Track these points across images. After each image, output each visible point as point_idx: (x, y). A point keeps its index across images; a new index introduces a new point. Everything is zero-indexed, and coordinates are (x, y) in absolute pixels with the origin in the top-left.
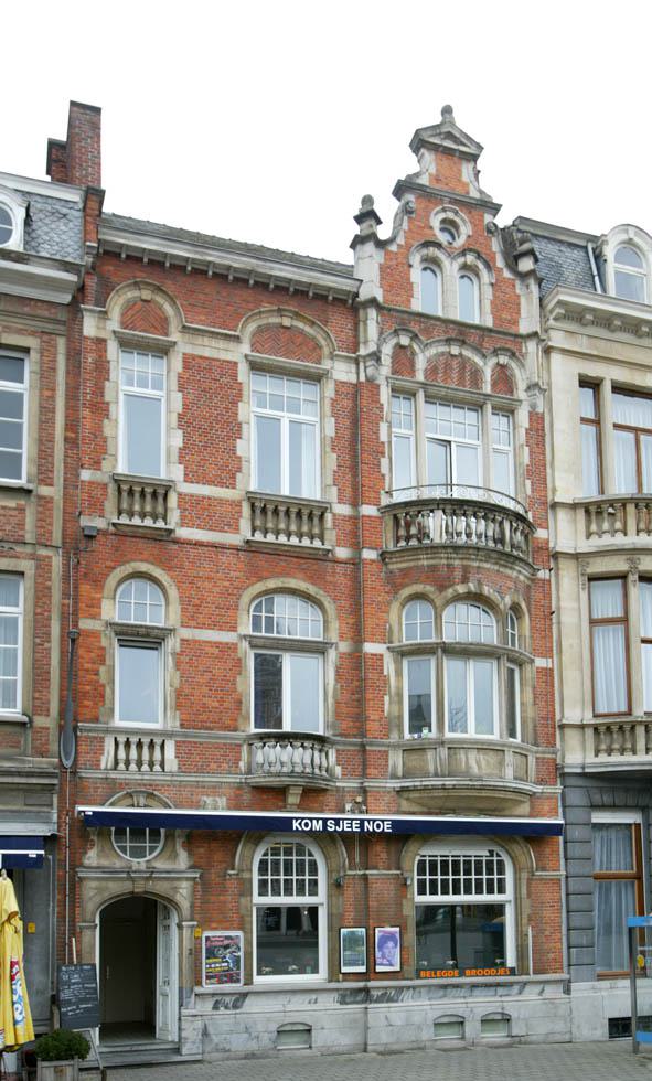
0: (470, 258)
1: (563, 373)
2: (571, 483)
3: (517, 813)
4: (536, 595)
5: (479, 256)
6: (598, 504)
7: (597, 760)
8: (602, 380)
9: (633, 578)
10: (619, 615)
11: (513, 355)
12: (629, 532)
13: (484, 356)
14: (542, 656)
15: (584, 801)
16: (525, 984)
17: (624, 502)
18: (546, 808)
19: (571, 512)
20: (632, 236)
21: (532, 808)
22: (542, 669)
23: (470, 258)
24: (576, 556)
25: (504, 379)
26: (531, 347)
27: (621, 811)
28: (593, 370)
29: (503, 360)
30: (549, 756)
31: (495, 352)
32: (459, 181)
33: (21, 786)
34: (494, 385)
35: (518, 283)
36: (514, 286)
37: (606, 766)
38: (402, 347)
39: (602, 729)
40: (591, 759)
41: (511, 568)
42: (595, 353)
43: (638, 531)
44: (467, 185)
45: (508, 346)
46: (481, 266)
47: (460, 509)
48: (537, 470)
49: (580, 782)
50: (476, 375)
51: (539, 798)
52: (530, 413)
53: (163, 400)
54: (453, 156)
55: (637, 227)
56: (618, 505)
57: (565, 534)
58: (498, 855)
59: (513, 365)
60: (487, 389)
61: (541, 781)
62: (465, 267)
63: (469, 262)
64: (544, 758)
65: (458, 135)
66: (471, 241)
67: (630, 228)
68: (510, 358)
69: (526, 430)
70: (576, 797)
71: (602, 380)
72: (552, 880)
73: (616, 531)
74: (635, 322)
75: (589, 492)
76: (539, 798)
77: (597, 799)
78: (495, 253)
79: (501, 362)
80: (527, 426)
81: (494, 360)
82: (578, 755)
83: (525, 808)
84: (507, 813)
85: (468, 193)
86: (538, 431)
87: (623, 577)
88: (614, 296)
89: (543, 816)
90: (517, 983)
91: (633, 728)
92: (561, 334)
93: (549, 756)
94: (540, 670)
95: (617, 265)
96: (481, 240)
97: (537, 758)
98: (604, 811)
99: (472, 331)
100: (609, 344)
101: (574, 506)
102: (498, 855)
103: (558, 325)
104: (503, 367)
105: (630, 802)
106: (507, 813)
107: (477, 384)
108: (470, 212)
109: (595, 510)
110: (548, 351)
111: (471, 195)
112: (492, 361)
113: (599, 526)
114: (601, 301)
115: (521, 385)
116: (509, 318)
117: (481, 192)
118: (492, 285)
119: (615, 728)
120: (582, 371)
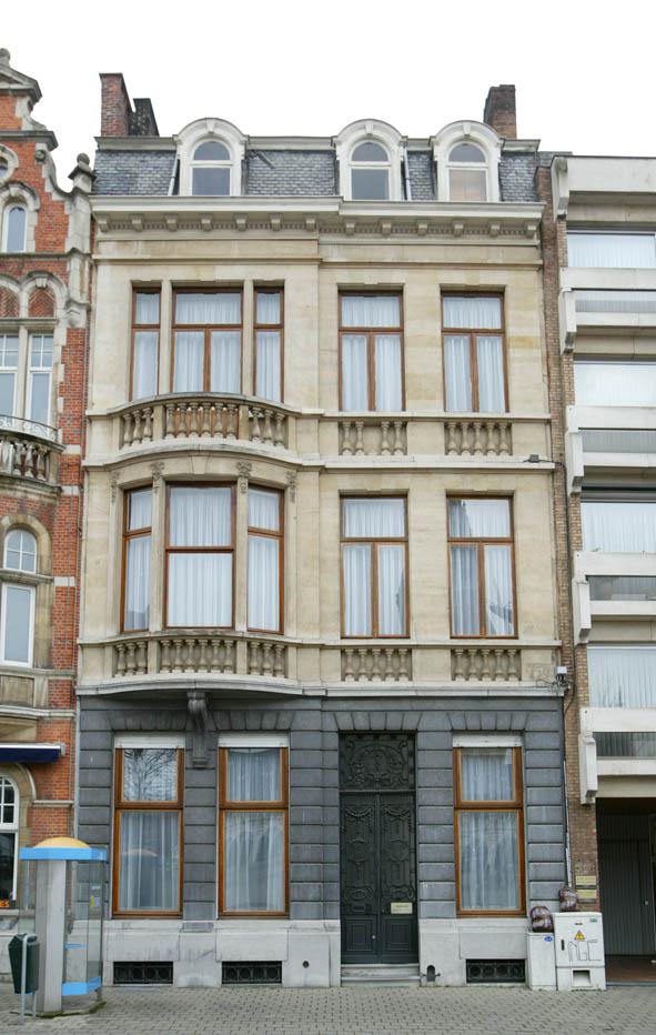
0: (14, 190)
1: (112, 287)
2: (105, 396)
3: (21, 738)
4: (62, 513)
5: (23, 186)
6: (129, 410)
7: (343, 684)
8: (160, 282)
9: (242, 482)
10: (505, 536)
11: (51, 276)
12: (155, 437)
13: (18, 283)
14: (63, 574)
15: (104, 725)
16: (17, 918)
17: (151, 405)
18: (57, 733)
19: (107, 423)
20: (211, 129)
21: (39, 733)
22: (63, 588)
23: (14, 190)
24: (107, 468)
25: (43, 301)
26: (75, 264)
27: (161, 735)
28: (146, 275)
29: (41, 282)
30: (65, 678)
31: (30, 276)
32: (11, 118)
33: (253, 751)
34: (32, 309)
35: (67, 205)
36: (63, 207)
37: (116, 687)
38: (42, 289)
39: (255, 645)
40: (108, 680)
41: (11, 489)
42: (148, 257)
43: (165, 434)
44: (21, 120)
45: (44, 268)
46: (26, 195)
47: (20, 442)
48: (75, 386)
49: (100, 705)
50: (12, 302)
51: (48, 722)
52: (68, 329)
53: (51, 376)
54: (6, 95)
55: (217, 119)
56: (232, 406)
57: (102, 446)
58: (7, 782)
59: (53, 285)
60: (24, 313)
61: (52, 704)
62: (11, 200)
63: (13, 194)
64: (58, 681)
65: (9, 75)
66: (19, 172)
67: (208, 122)
68: (48, 279)
69: (63, 347)
70: (96, 721)
71: (160, 282)
72: (56, 809)
73: (191, 432)
74: (376, 221)
75: (120, 403)
76: (48, 722)
77: (120, 722)
78: (44, 180)
79: (39, 285)
80: (64, 343)
81: (31, 284)
82: (96, 676)
83: (31, 733)
84: (10, 738)
85: (20, 128)
86: (79, 345)
87: (229, 482)
88: (448, 200)
89: (51, 742)
90: (7, 917)
91: (285, 650)
92: (111, 245)
93: (65, 678)
94: (60, 590)
95: (452, 164)
96: (30, 170)
97: (50, 681)
98: (129, 735)
99: (11, 260)
100: (170, 244)
101: (110, 417)
102: (7, 782)
103: (108, 236)
104: (43, 289)
105: (161, 725)
106: (10, 738)
107: (12, 311)
108: (20, 146)
109: (132, 417)
110: (95, 265)
111: (24, 128)
112: (29, 286)
113: (141, 430)
114: (176, 204)
115: (60, 303)
116: (54, 239)
117: (34, 123)
118: (37, 211)
119: (268, 647)
120: (134, 279)
